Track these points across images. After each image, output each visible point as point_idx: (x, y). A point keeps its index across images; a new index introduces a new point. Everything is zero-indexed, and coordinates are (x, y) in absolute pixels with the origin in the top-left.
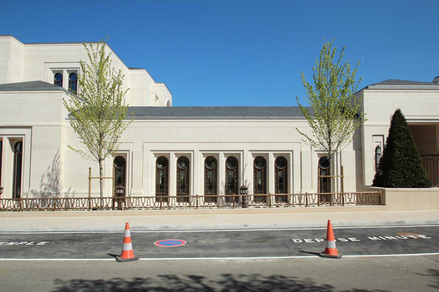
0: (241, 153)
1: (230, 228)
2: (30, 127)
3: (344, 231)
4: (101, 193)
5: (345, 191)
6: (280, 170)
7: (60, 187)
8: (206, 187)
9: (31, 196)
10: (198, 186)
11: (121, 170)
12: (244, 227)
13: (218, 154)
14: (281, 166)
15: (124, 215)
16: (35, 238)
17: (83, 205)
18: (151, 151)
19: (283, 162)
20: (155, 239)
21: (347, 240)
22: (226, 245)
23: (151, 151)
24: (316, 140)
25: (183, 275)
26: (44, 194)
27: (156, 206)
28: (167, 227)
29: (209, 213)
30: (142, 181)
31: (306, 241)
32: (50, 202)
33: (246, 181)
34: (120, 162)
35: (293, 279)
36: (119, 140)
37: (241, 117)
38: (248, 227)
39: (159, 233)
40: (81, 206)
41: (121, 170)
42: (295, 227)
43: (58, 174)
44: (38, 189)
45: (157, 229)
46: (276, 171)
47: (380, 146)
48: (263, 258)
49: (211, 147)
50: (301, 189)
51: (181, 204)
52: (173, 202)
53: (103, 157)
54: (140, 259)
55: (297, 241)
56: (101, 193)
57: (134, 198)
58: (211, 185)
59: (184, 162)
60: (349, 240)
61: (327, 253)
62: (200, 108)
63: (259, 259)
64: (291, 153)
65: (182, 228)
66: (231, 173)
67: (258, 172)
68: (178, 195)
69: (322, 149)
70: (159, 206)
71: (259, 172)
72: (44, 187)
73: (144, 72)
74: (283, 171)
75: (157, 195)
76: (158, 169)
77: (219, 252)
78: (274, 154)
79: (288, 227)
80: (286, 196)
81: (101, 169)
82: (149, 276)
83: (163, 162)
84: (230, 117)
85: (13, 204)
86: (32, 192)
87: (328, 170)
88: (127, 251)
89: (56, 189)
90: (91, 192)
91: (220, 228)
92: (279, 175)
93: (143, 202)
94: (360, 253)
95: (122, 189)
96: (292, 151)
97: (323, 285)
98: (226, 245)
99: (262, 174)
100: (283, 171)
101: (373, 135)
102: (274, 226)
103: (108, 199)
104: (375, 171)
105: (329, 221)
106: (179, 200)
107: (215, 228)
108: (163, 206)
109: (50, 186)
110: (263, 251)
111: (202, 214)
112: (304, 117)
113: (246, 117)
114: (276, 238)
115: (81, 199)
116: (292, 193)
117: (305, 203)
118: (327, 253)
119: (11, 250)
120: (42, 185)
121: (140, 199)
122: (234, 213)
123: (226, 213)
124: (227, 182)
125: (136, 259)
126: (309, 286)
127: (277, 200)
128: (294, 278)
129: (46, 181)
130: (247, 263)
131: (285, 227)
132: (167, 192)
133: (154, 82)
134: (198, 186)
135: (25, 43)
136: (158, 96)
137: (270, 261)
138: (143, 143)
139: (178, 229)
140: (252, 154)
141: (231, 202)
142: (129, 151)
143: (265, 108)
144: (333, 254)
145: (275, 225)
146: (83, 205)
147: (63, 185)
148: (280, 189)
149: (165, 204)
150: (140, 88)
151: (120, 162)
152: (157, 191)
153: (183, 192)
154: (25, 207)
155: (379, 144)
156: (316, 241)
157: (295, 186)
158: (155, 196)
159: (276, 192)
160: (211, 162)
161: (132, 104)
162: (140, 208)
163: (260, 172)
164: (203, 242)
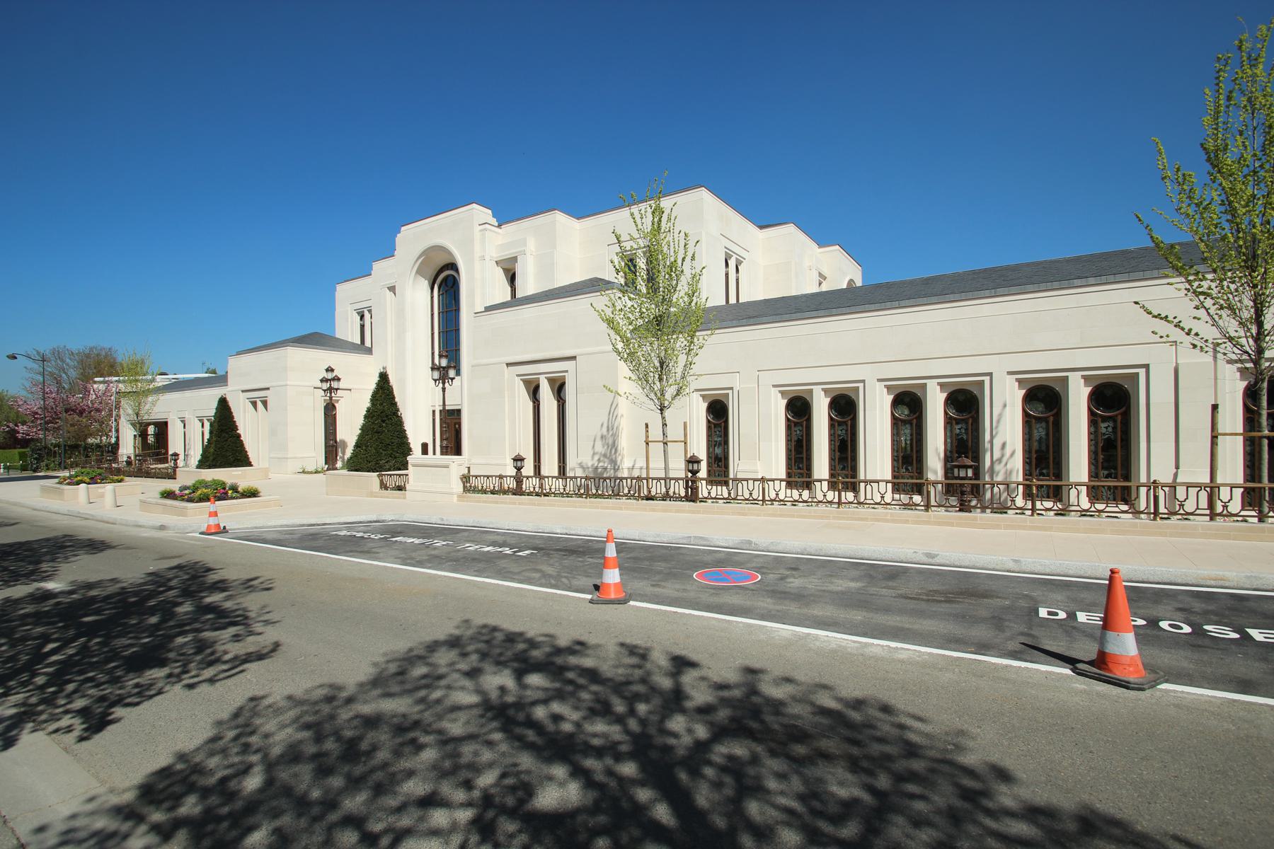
1: (888, 556)
2: (574, 358)
3: (1251, 604)
4: (666, 469)
5: (1219, 480)
6: (1104, 419)
7: (619, 459)
9: (579, 473)
10: (876, 454)
11: (719, 425)
12: (925, 559)
13: (924, 386)
14: (1107, 407)
15: (693, 512)
16: (520, 541)
18: (1010, 373)
20: (696, 568)
21: (1236, 636)
22: (847, 600)
23: (1010, 373)
24: (1210, 333)
26: (597, 468)
28: (750, 542)
29: (866, 519)
30: (760, 448)
31: (1082, 617)
32: (603, 484)
33: (1004, 445)
34: (718, 411)
35: (909, 722)
36: (695, 369)
37: (987, 293)
38: (937, 560)
41: (719, 425)
42: (1082, 573)
43: (615, 436)
44: (590, 462)
45: (731, 544)
48: (893, 644)
49: (906, 372)
50: (1177, 467)
52: (821, 489)
53: (666, 403)
54: (632, 603)
55: (1057, 614)
56: (666, 469)
57: (1189, 486)
58: (908, 458)
59: (845, 407)
61: (1100, 666)
62: (889, 285)
63: (879, 646)
64: (1142, 372)
65: (780, 548)
69: (1234, 357)
70: (836, 500)
72: (596, 458)
73: (790, 229)
75: (832, 475)
76: (896, 422)
77: (805, 611)
79: (1058, 571)
80: (1128, 489)
81: (665, 425)
82: (602, 642)
83: (799, 408)
84: (957, 296)
85: (558, 485)
86: (581, 465)
88: (609, 585)
89: (614, 462)
90: (651, 466)
91: (866, 555)
92: (1104, 430)
94: (1246, 686)
95: (970, 467)
96: (990, 374)
97: (986, 763)
98: (847, 600)
99: (1047, 429)
100: (1115, 421)
102: (1011, 565)
103: (751, 482)
106: (833, 486)
107: (852, 554)
108: (843, 500)
109: (605, 456)
110: (916, 627)
111: (848, 519)
112: (1169, 271)
113: (1000, 291)
114: (991, 597)
115: (747, 480)
116: (1143, 479)
118: (1100, 666)
119: (474, 559)
120: (594, 454)
122: (928, 523)
123: (906, 522)
124: (944, 447)
125: (623, 602)
126: (938, 756)
127: (1028, 495)
128: (920, 719)
129: (599, 448)
130: (839, 655)
131: (1048, 571)
132: (809, 468)
133: (814, 245)
134: (876, 454)
135: (579, 218)
136: (825, 273)
137: (903, 656)
138: (757, 373)
139: (771, 548)
142: (731, 388)
143: (1068, 261)
144: (1119, 674)
145: (1015, 561)
147: (625, 452)
148: (1103, 468)
149: (850, 496)
150: (786, 259)
151: (718, 411)
152: (789, 466)
153: (843, 469)
154: (626, 491)
157: (1155, 459)
158: (827, 477)
159: (1093, 475)
160: (908, 404)
161: (760, 296)
163: (1044, 425)
164: (795, 583)
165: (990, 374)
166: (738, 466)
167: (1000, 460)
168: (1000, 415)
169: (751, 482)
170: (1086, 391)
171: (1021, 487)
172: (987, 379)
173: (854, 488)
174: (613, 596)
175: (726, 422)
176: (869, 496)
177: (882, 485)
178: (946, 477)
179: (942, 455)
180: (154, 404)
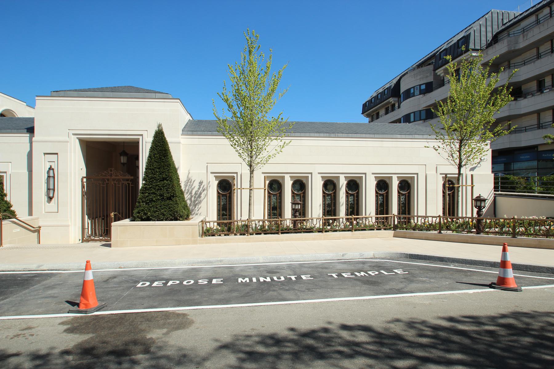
6: (351, 195)
13: (283, 178)
19: (406, 185)
25: (20, 330)
39: (377, 262)
46: (347, 197)
51: (101, 238)
64: (364, 176)
66: (274, 199)
67: (221, 198)
71: (327, 198)
74: (354, 196)
78: (398, 177)
87: (228, 195)
96: (311, 173)
99: (383, 198)
101: (45, 154)
104: (46, 197)
140: (216, 177)
142: (237, 173)
156: (356, 275)
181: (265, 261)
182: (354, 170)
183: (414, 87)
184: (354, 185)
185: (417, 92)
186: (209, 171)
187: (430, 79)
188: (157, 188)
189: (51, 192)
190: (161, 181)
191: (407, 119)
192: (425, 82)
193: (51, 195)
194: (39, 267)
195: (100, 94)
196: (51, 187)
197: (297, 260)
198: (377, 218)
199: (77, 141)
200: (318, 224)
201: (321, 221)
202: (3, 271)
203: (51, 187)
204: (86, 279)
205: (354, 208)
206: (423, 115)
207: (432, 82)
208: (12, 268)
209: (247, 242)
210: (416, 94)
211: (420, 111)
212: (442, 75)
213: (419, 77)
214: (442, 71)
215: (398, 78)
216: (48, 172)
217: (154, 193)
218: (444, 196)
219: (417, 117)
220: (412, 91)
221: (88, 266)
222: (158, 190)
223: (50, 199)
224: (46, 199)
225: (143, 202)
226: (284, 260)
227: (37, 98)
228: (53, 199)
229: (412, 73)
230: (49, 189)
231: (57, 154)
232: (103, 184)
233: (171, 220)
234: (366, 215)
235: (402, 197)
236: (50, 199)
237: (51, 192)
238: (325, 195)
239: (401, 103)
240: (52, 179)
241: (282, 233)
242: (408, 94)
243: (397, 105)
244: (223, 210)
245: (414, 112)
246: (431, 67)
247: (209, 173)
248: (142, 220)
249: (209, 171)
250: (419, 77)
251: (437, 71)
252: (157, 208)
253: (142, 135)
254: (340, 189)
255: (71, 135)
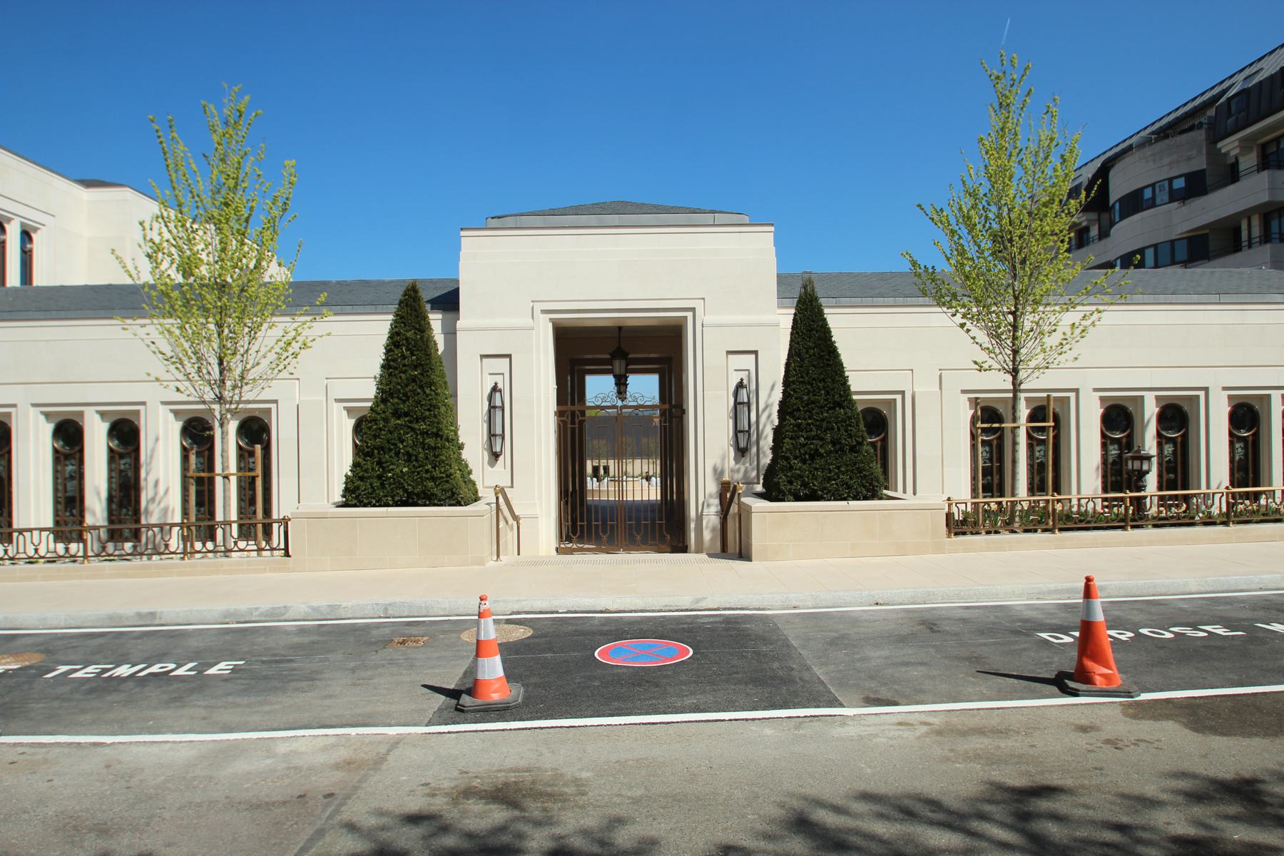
0: (1202, 394)
8: (56, 502)
13: (81, 414)
15: (1214, 541)
17: (36, 550)
27: (172, 549)
33: (156, 483)
40: (31, 552)
47: (745, 382)
49: (65, 396)
60: (1139, 635)
68: (57, 523)
70: (81, 554)
74: (1175, 446)
78: (1157, 398)
87: (995, 442)
93: (36, 541)
96: (1077, 391)
99: (1246, 448)
104: (486, 454)
105: (1088, 579)
117: (282, 546)
121: (27, 534)
141: (127, 540)
142: (903, 393)
146: (36, 550)
155: (744, 375)
162: (31, 561)
165: (1077, 391)
166: (283, 504)
167: (153, 499)
168: (153, 450)
169: (36, 533)
170: (104, 427)
171: (176, 529)
172: (1072, 395)
173: (136, 535)
174: (495, 697)
175: (81, 451)
176: (21, 550)
177: (36, 533)
178: (111, 521)
179: (104, 494)
180: (288, 350)
181: (1202, 589)
182: (1177, 380)
183: (1153, 185)
184: (1177, 416)
185: (1163, 196)
186: (332, 396)
187: (1199, 163)
188: (824, 425)
189: (499, 440)
190: (830, 408)
191: (1127, 261)
192: (1185, 170)
193: (498, 449)
194: (698, 601)
195: (593, 219)
196: (499, 431)
197: (1274, 586)
198: (1161, 498)
199: (550, 325)
200: (1218, 506)
201: (1224, 499)
202: (642, 611)
203: (499, 431)
204: (482, 638)
205: (1179, 471)
206: (1182, 253)
207: (1203, 171)
208: (640, 604)
209: (966, 551)
210: (1158, 201)
211: (1172, 242)
212: (1233, 153)
213: (1166, 160)
214: (1237, 144)
215: (1098, 164)
216: (490, 398)
217: (817, 437)
218: (974, 447)
219: (1165, 254)
220: (1148, 194)
221: (1088, 592)
222: (827, 429)
223: (495, 456)
224: (732, 454)
225: (796, 458)
226: (1245, 587)
227: (463, 233)
228: (501, 458)
229: (1148, 151)
230: (491, 435)
231: (509, 356)
232: (573, 422)
233: (866, 498)
234: (1208, 487)
235: (1237, 446)
236: (495, 456)
237: (499, 440)
238: (1106, 441)
239: (1112, 224)
240: (499, 413)
241: (1133, 527)
242: (1134, 203)
243: (1094, 232)
244: (1168, 472)
245: (1155, 246)
246: (1200, 136)
247: (331, 401)
248: (798, 498)
249: (332, 396)
250: (1166, 160)
251: (1219, 145)
252: (830, 471)
253: (693, 310)
254: (1144, 428)
255: (537, 311)
